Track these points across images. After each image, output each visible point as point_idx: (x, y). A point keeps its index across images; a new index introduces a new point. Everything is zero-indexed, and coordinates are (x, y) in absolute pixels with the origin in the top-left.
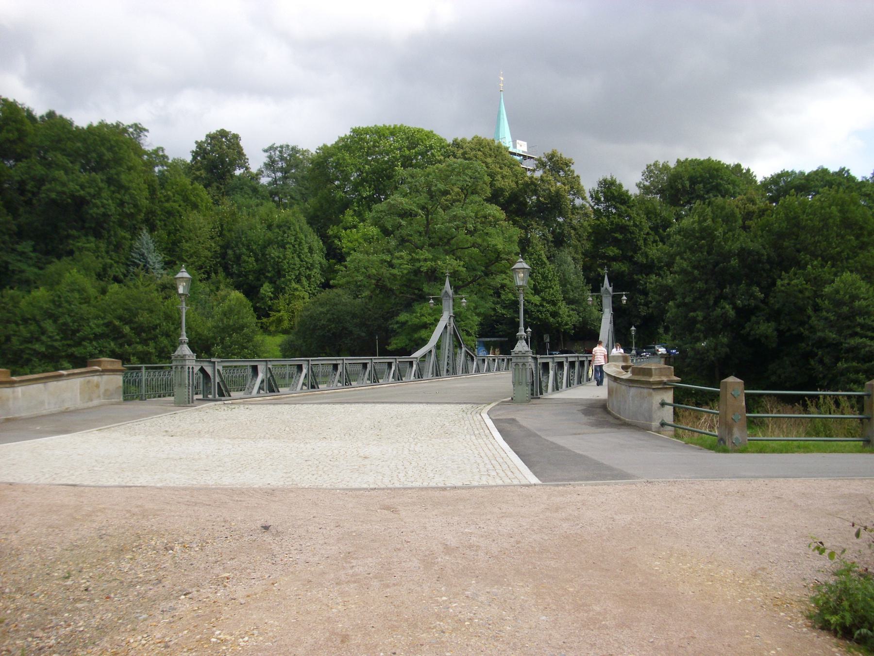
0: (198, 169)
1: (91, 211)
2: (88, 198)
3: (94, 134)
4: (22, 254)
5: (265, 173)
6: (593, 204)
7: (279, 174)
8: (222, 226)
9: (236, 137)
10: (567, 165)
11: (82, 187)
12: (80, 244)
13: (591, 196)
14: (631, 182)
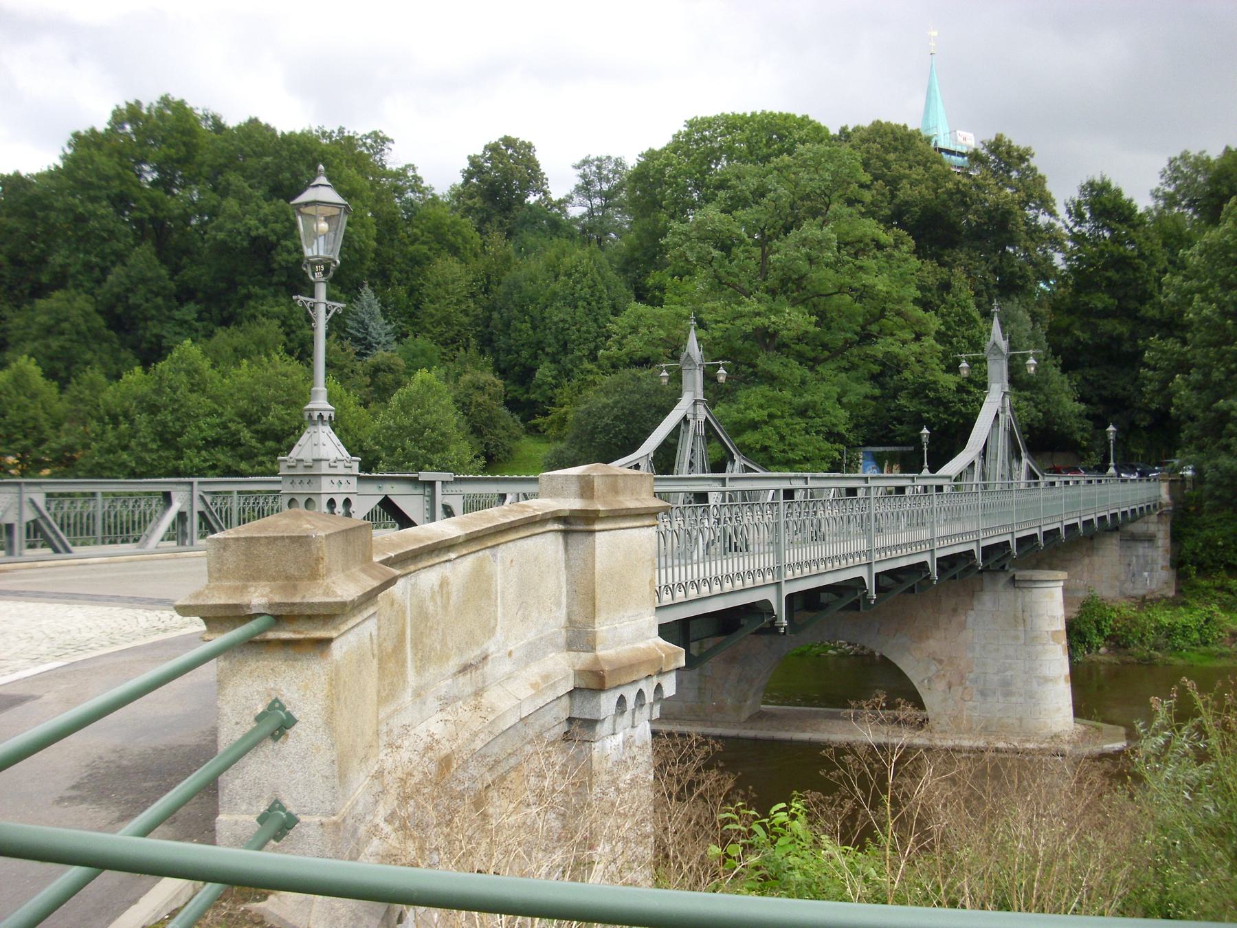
0: (471, 197)
1: (279, 258)
2: (273, 238)
3: (290, 144)
4: (182, 323)
5: (576, 199)
6: (1071, 224)
7: (597, 201)
8: (488, 278)
9: (529, 147)
10: (1022, 158)
11: (264, 222)
12: (265, 308)
13: (1069, 211)
14: (1142, 188)
